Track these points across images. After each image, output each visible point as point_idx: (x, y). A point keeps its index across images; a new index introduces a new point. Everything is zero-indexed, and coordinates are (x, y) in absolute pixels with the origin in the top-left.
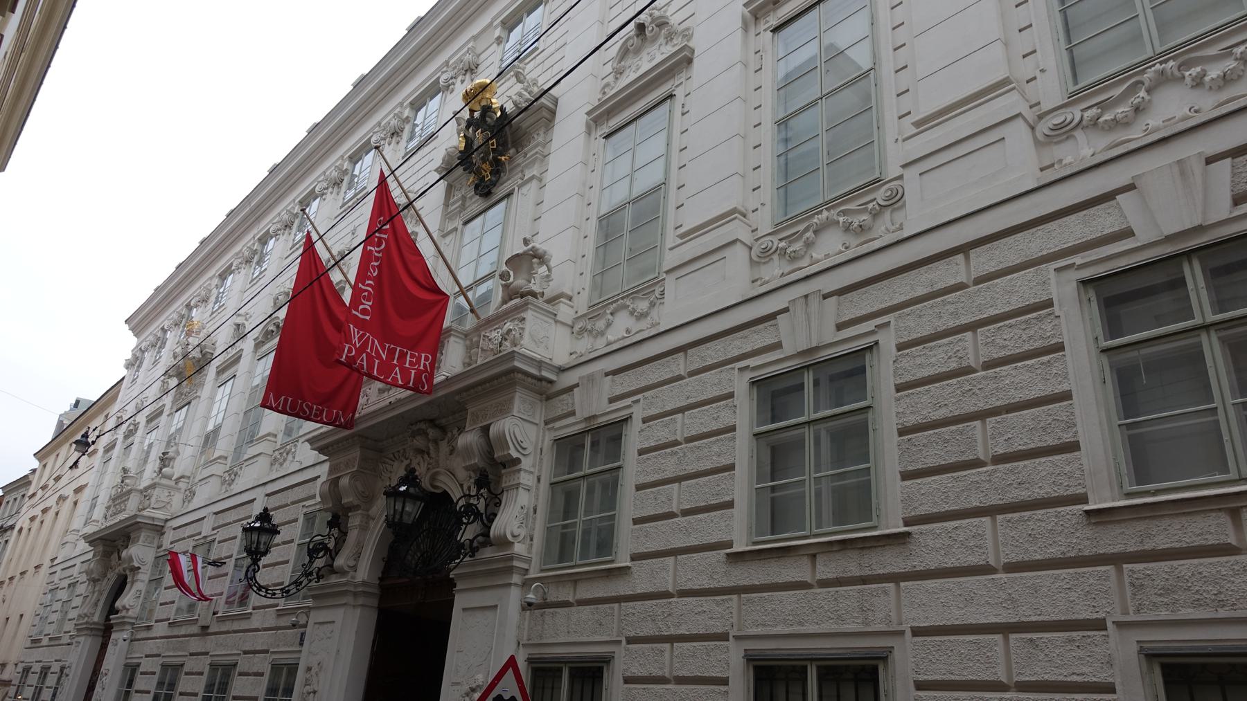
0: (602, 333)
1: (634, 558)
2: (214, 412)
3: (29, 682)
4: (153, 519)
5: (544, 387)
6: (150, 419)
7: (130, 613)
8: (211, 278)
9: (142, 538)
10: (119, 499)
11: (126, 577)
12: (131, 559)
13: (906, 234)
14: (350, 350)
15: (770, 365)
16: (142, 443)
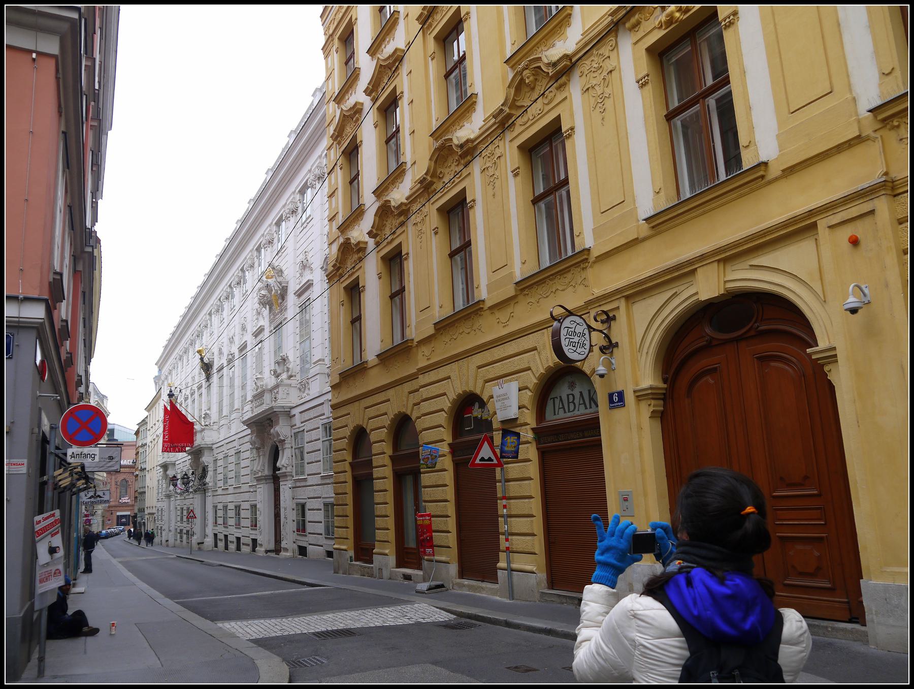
6: (245, 347)
10: (259, 396)
11: (277, 447)
12: (278, 435)
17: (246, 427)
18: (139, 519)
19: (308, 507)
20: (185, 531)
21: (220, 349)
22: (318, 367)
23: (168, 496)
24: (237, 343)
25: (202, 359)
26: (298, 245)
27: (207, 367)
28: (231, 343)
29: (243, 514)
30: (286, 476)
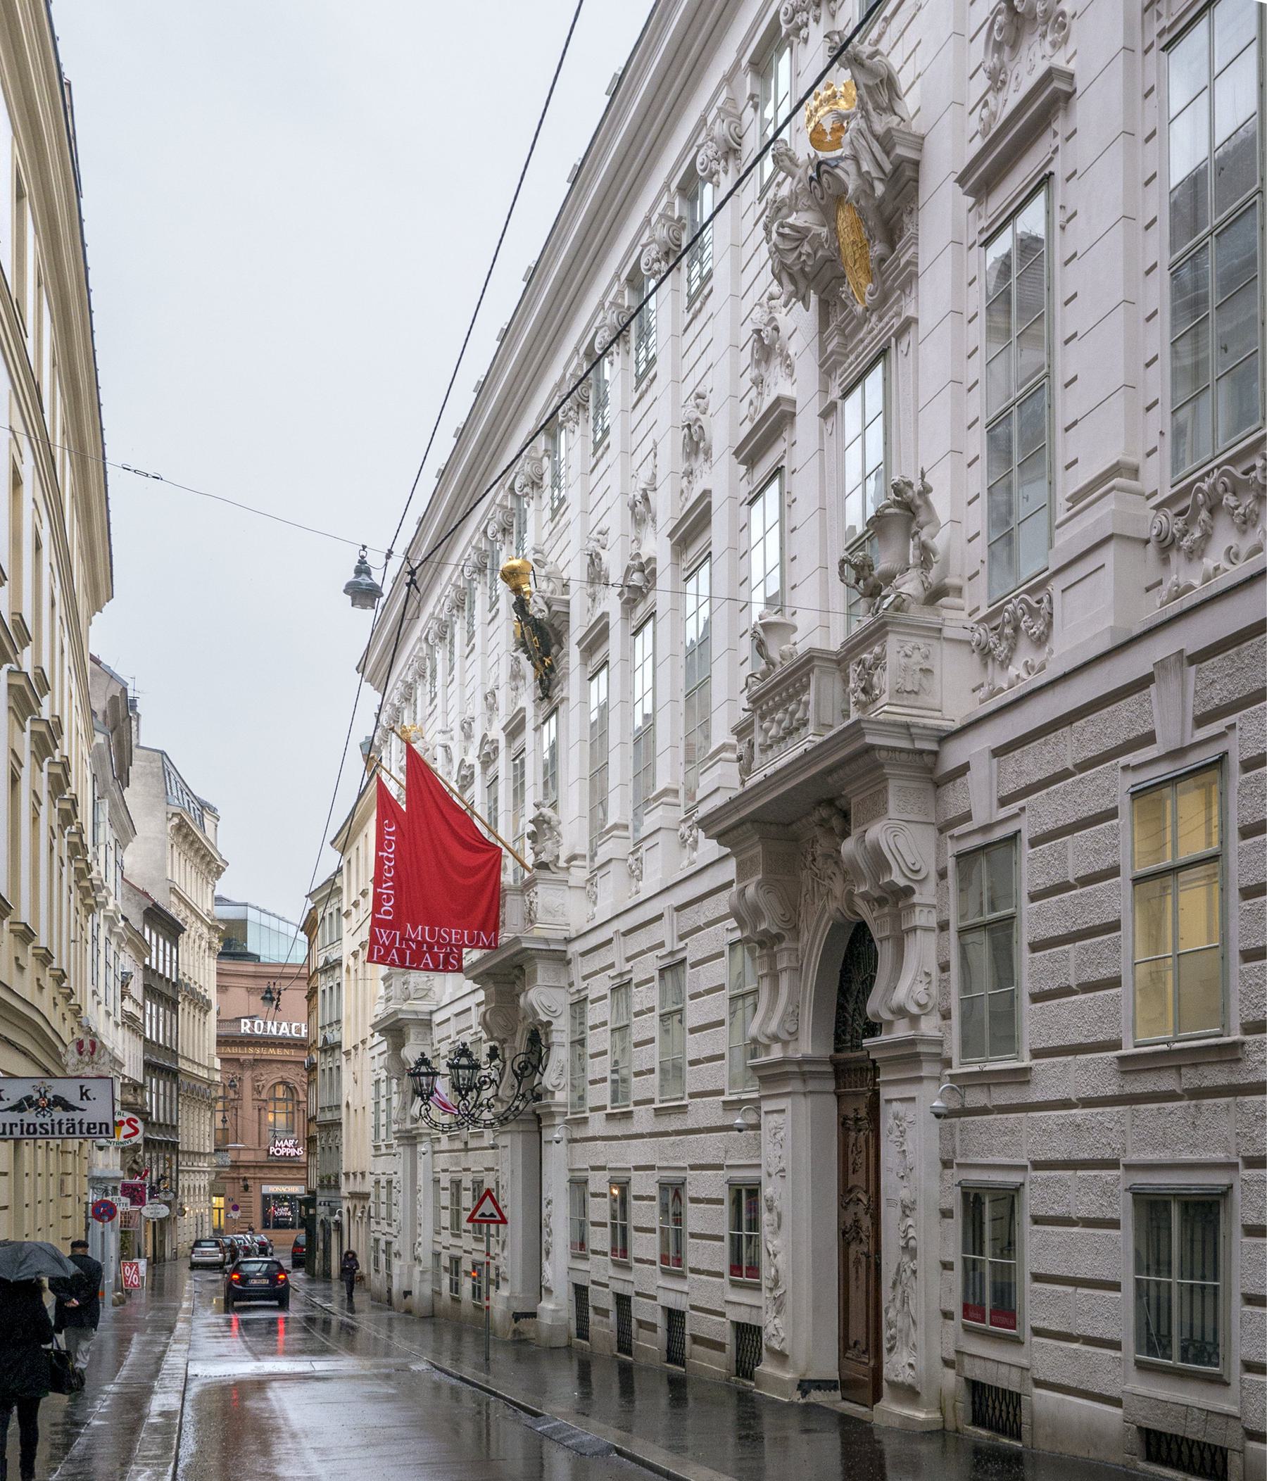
3: (593, 1216)
4: (416, 1012)
5: (930, 768)
8: (728, 79)
9: (412, 1037)
10: (780, 689)
12: (879, 861)
13: (642, 897)
14: (379, 951)
16: (585, 702)
21: (446, 747)
23: (410, 1139)
24: (667, 509)
25: (521, 606)
27: (541, 639)
28: (639, 521)
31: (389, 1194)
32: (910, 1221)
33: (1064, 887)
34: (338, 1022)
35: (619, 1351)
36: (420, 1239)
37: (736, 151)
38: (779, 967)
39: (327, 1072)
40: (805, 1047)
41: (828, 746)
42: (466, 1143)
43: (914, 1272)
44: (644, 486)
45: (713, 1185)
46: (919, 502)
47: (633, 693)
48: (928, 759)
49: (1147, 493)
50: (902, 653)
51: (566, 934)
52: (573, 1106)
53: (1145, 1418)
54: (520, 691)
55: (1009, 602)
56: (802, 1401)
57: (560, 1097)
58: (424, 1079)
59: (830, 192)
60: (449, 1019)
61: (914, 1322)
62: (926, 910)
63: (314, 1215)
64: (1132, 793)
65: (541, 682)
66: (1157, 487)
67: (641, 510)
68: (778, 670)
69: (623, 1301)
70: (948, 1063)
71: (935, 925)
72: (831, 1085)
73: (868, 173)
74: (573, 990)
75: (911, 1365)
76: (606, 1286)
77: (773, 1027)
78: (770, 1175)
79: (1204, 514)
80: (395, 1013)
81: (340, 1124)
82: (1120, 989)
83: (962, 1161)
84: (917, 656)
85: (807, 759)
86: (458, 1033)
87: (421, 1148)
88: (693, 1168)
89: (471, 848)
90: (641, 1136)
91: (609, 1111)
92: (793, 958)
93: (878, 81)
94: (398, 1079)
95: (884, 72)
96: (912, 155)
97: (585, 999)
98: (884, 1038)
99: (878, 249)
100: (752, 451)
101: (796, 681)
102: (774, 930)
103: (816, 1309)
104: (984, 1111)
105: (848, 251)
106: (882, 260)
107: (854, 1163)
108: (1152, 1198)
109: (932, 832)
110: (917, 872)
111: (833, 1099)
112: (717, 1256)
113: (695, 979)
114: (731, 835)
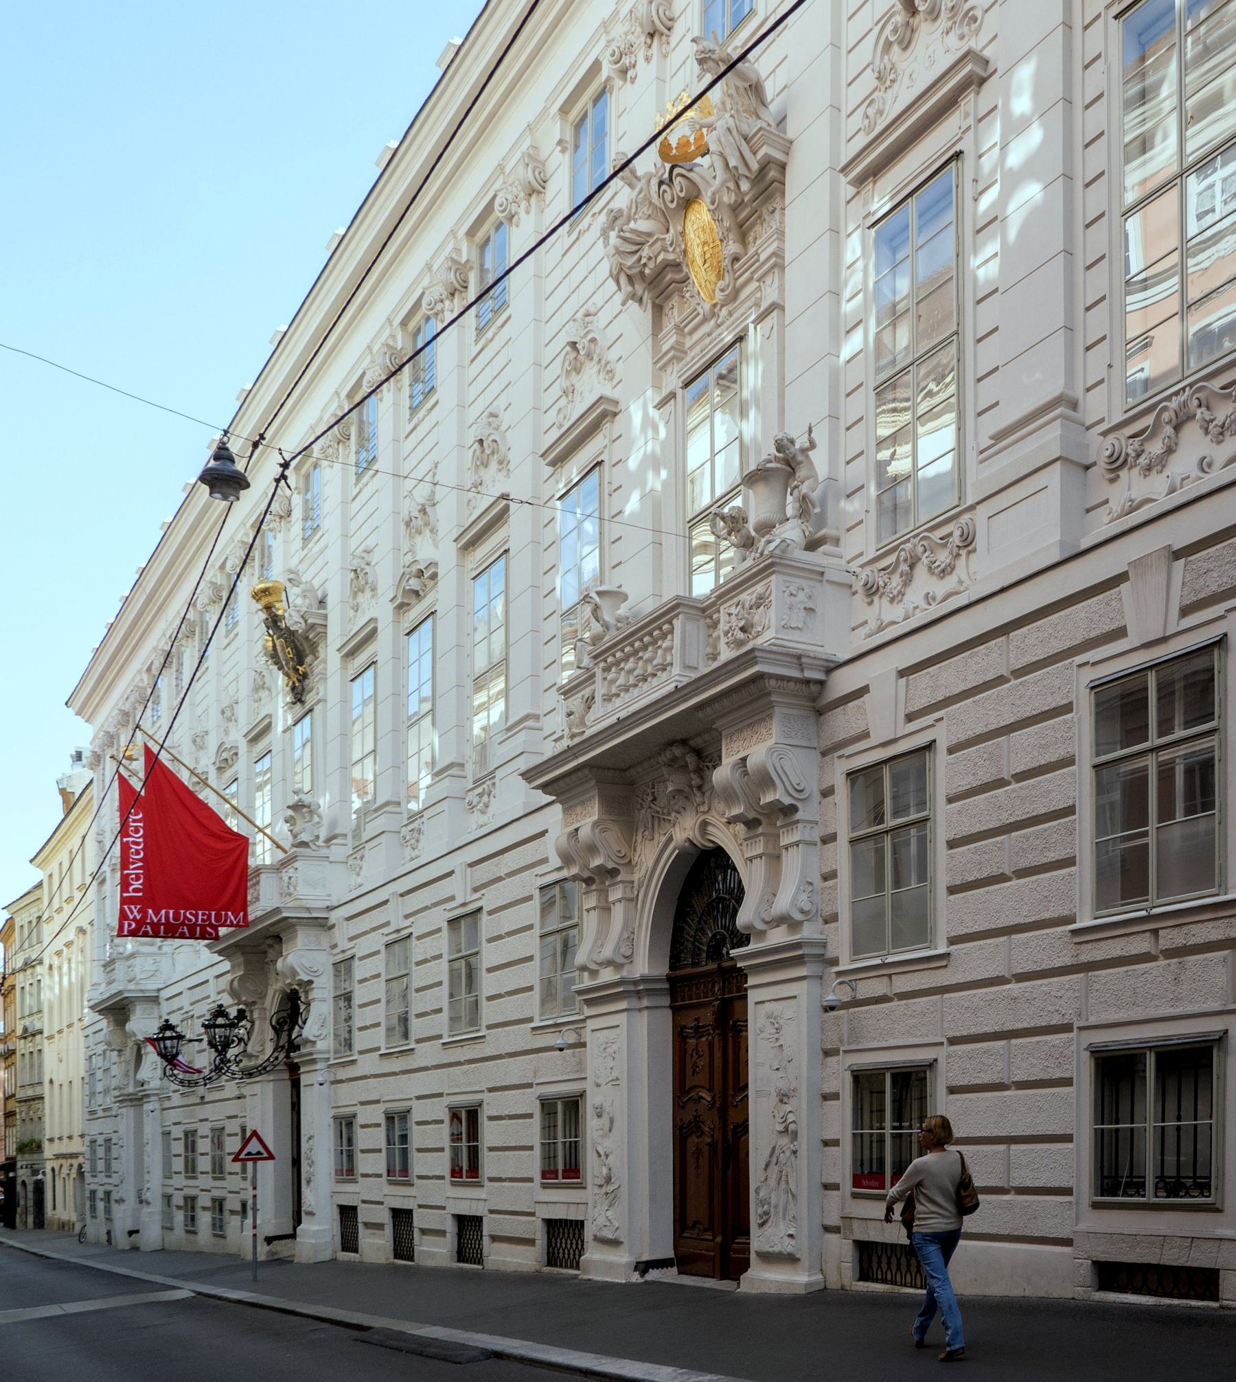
0: (1161, 462)
1: (953, 941)
2: (413, 685)
4: (142, 991)
5: (812, 694)
6: (267, 729)
7: (152, 1085)
12: (294, 973)
14: (130, 925)
15: (1115, 661)
17: (217, 958)
18: (22, 1174)
19: (486, 1112)
20: (100, 1194)
22: (382, 819)
23: (136, 1100)
24: (245, 721)
25: (273, 621)
26: (473, 391)
27: (294, 651)
29: (364, 1138)
30: (314, 1061)
31: (108, 1150)
32: (788, 1108)
33: (1000, 783)
34: (40, 1011)
35: (395, 1257)
36: (148, 1185)
37: (539, 192)
38: (611, 899)
39: (27, 1056)
40: (642, 967)
41: (741, 661)
42: (203, 1098)
43: (795, 1152)
44: (422, 501)
45: (376, 1114)
46: (800, 458)
47: (405, 686)
48: (814, 688)
49: (1087, 424)
50: (787, 593)
51: (328, 903)
52: (336, 1052)
53: (1103, 1253)
54: (263, 702)
55: (908, 541)
56: (641, 1280)
57: (320, 1045)
58: (168, 1043)
59: (682, 195)
60: (181, 993)
61: (793, 1196)
62: (809, 826)
63: (14, 1178)
64: (1092, 688)
65: (293, 688)
66: (1106, 415)
67: (228, 714)
68: (613, 632)
69: (402, 1217)
70: (835, 962)
71: (818, 839)
72: (666, 1001)
73: (736, 168)
74: (337, 951)
75: (791, 1236)
76: (382, 1203)
77: (607, 952)
78: (598, 1085)
79: (1169, 430)
80: (120, 992)
81: (42, 1098)
82: (1073, 868)
83: (1082, 1024)
84: (801, 596)
85: (678, 696)
86: (192, 1004)
87: (147, 1107)
88: (491, 1090)
89: (214, 835)
90: (425, 1069)
91: (383, 1051)
92: (628, 890)
93: (747, 85)
94: (120, 1051)
95: (753, 76)
96: (779, 156)
97: (352, 957)
98: (753, 946)
99: (733, 247)
100: (408, 598)
101: (655, 629)
102: (610, 865)
103: (653, 1198)
104: (883, 999)
105: (696, 252)
106: (736, 259)
107: (695, 1065)
108: (1104, 1055)
109: (815, 755)
110: (801, 791)
111: (669, 1013)
112: (378, 1164)
113: (419, 950)
114: (555, 786)
